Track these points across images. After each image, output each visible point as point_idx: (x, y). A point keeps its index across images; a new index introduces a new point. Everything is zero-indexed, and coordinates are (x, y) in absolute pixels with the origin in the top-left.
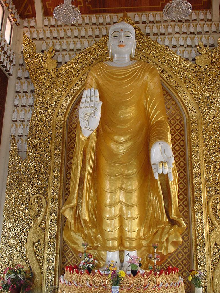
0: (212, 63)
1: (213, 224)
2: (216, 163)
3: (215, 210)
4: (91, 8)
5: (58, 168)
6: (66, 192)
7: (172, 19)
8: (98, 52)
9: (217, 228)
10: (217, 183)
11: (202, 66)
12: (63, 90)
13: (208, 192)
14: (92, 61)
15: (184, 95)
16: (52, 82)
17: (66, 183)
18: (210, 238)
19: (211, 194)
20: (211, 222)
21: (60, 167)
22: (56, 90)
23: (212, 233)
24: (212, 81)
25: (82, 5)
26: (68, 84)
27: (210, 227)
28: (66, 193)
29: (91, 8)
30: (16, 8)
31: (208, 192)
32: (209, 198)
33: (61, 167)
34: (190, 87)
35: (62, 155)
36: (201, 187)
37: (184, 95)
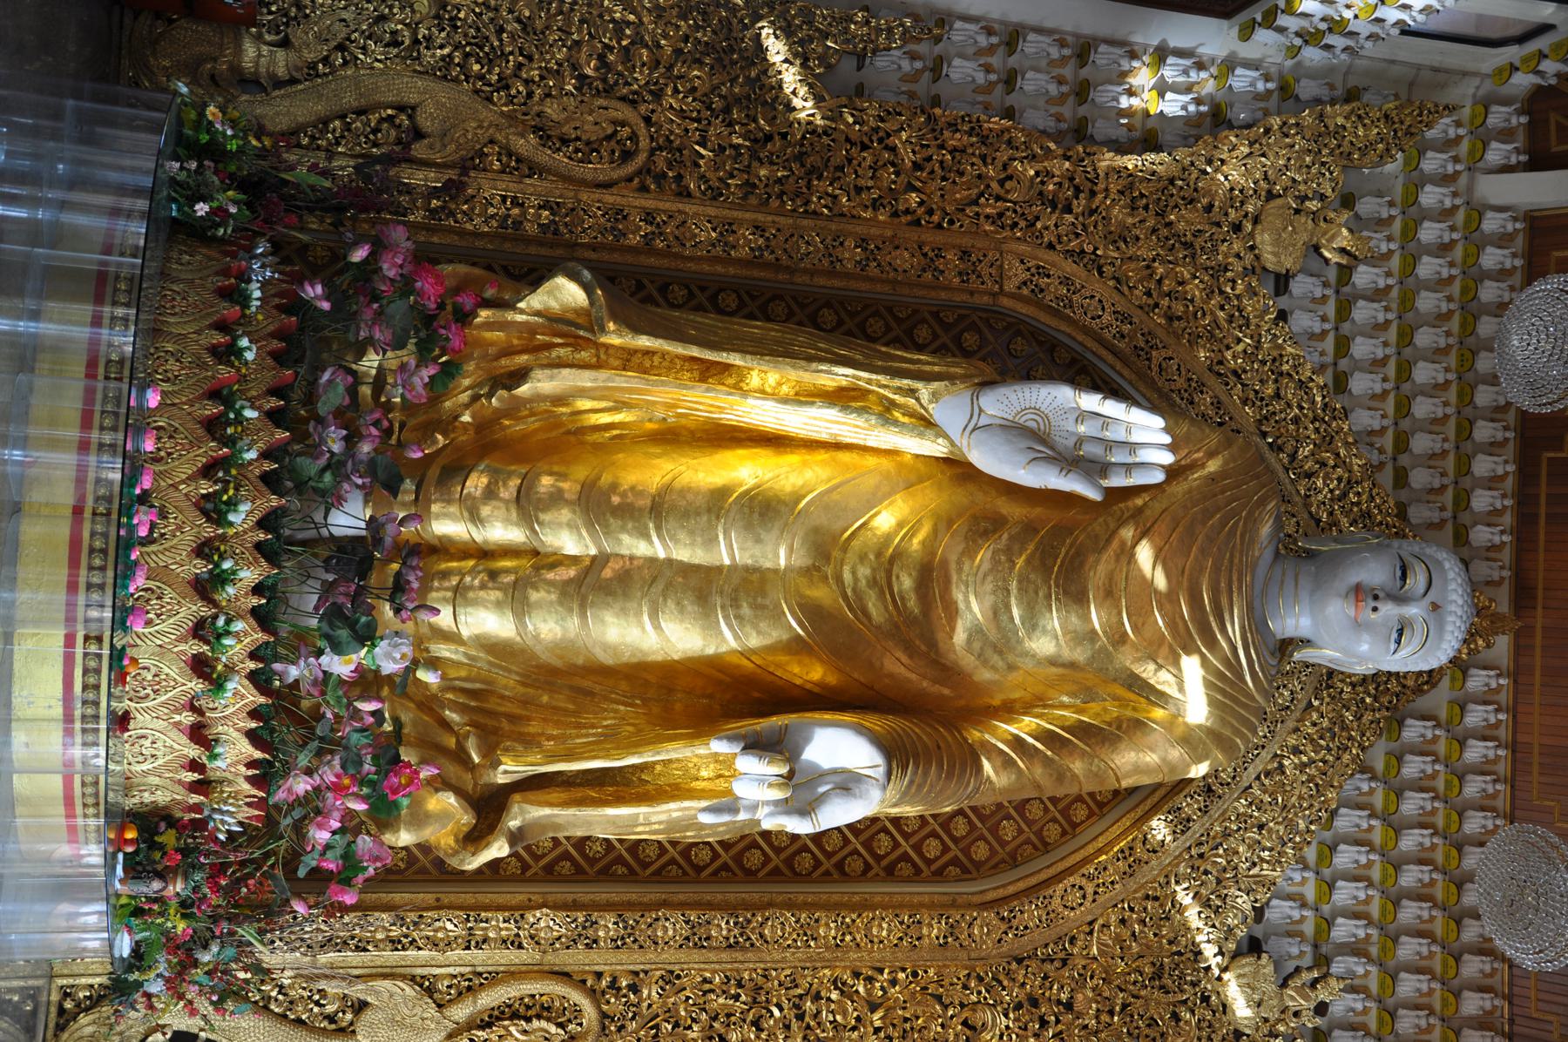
15: (1090, 890)
20: (469, 989)
37: (1090, 890)
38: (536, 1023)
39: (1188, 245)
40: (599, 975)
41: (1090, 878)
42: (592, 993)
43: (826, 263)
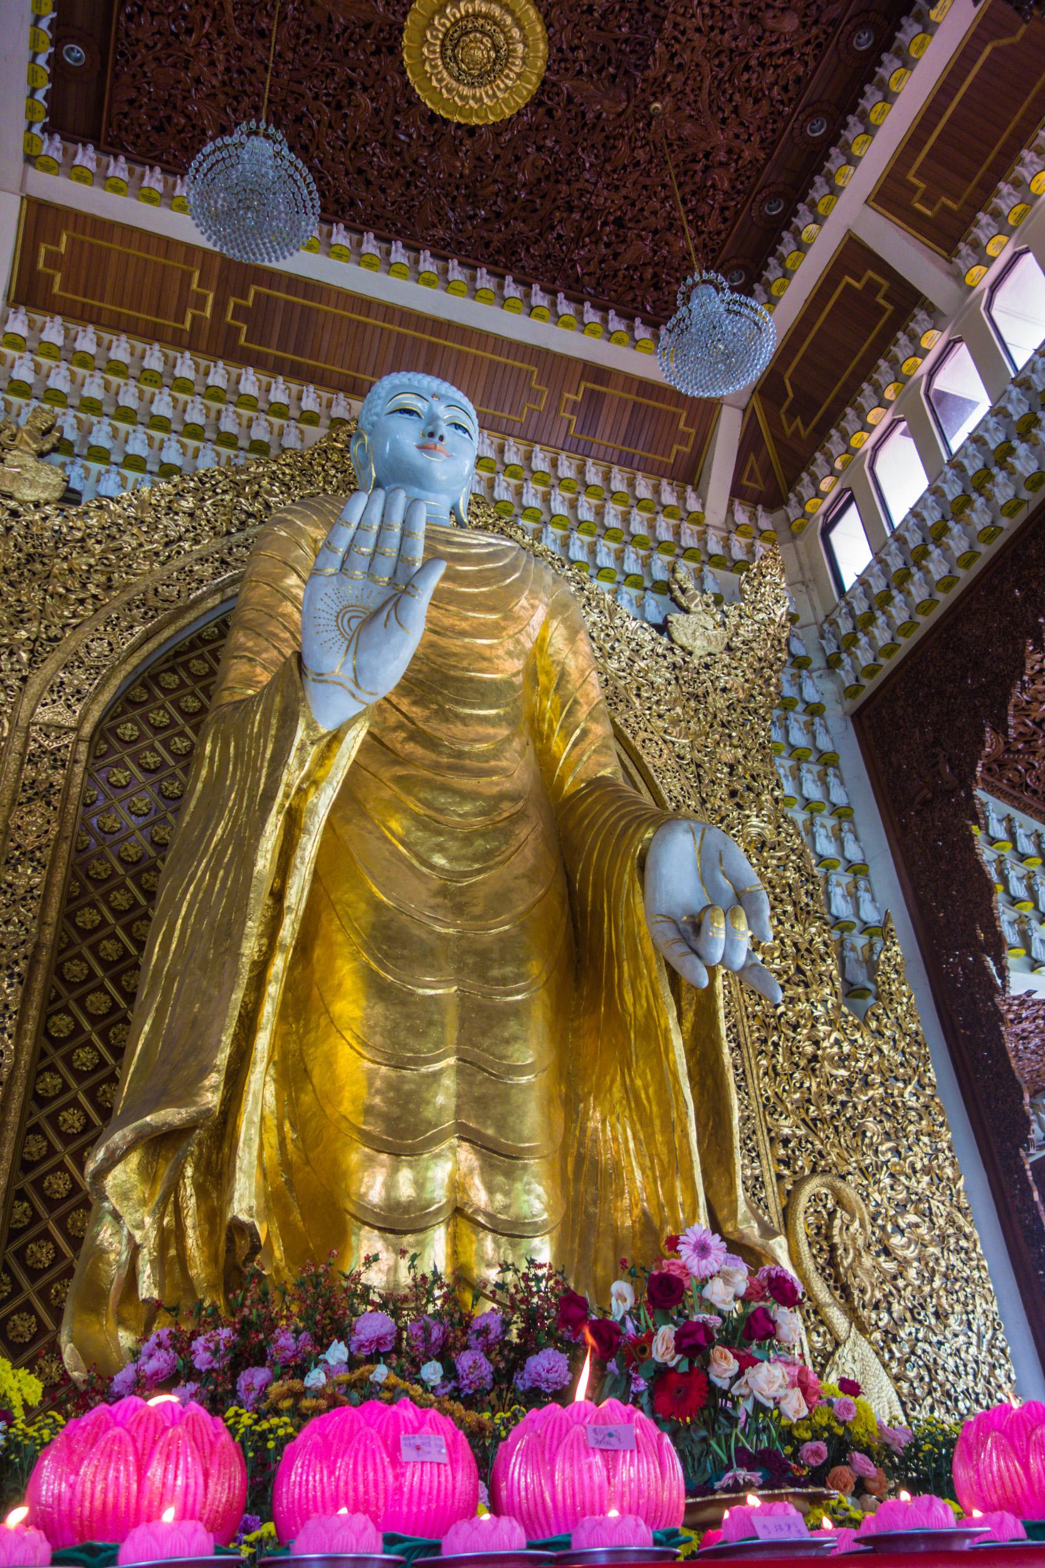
0: (729, 648)
1: (822, 1322)
2: (794, 1031)
3: (821, 1250)
4: (243, 338)
5: (16, 963)
6: (31, 1114)
7: (401, 499)
8: (270, 493)
9: (849, 1344)
10: (814, 1120)
11: (698, 652)
12: (82, 602)
13: (780, 1161)
14: (243, 523)
15: (643, 735)
16: (29, 555)
17: (41, 1066)
18: (854, 1310)
19: (795, 1173)
20: (816, 1313)
21: (25, 957)
22: (46, 591)
23: (828, 1370)
24: (739, 710)
25: (208, 313)
26: (115, 584)
27: (815, 1337)
28: (29, 1124)
29: (243, 338)
30: (240, 263)
31: (780, 1161)
32: (789, 1192)
33: (32, 960)
34: (660, 716)
35: (45, 899)
36: (754, 1132)
37: (643, 735)
38: (837, 1240)
39: (30, 558)
40: (780, 1177)
41: (635, 734)
42: (799, 1184)
43: (33, 905)
